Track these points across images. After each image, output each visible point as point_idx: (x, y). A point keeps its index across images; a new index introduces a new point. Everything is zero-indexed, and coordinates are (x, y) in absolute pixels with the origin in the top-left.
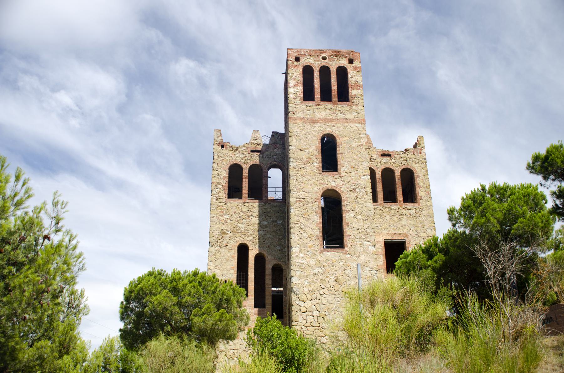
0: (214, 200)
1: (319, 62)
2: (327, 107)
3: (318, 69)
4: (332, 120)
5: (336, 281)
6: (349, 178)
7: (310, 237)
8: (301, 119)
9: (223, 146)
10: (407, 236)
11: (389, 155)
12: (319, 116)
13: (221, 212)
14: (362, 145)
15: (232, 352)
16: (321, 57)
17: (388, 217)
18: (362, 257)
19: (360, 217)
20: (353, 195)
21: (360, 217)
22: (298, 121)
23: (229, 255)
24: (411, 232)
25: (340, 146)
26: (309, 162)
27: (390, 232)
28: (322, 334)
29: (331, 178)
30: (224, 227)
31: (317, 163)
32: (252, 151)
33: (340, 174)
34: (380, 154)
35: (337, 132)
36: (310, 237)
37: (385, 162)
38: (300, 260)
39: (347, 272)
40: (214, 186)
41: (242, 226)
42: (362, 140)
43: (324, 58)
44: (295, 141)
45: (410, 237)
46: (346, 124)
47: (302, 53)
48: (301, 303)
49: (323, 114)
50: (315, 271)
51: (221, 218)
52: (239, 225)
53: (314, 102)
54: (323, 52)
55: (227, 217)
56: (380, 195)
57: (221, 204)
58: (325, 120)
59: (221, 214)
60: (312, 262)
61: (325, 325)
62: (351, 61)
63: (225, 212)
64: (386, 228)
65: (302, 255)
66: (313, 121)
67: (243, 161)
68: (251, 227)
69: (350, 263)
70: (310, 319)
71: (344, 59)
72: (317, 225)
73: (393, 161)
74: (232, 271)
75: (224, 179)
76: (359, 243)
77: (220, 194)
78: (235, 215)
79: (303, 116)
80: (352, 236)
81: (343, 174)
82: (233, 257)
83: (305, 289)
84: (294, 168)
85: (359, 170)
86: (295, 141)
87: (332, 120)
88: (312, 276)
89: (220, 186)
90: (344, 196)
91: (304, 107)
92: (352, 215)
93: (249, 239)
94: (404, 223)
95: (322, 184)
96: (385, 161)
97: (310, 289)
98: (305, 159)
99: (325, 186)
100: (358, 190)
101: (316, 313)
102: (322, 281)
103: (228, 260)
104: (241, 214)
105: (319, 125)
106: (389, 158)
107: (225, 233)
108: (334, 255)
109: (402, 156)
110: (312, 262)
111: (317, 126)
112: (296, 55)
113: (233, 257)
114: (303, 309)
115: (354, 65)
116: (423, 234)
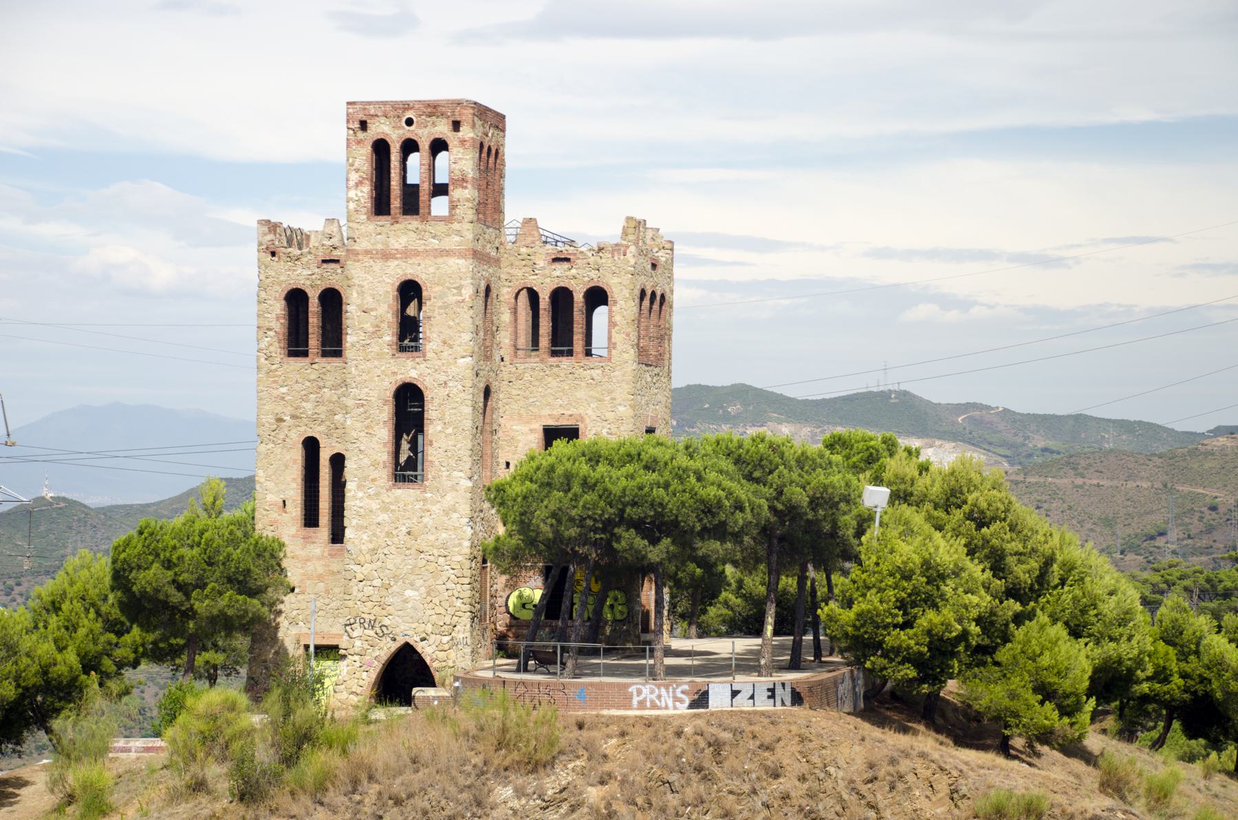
0: (262, 360)
1: (401, 132)
2: (410, 227)
3: (398, 146)
4: (417, 253)
5: (409, 533)
6: (439, 362)
7: (375, 464)
8: (367, 252)
9: (273, 254)
10: (582, 419)
11: (567, 260)
12: (397, 246)
13: (275, 382)
14: (463, 301)
15: (295, 613)
16: (404, 120)
17: (554, 383)
18: (449, 497)
19: (450, 430)
20: (443, 392)
21: (450, 430)
22: (360, 257)
23: (288, 457)
24: (590, 412)
25: (428, 303)
26: (377, 333)
27: (555, 413)
28: (384, 613)
29: (410, 363)
30: (279, 409)
31: (389, 336)
32: (324, 261)
33: (424, 356)
34: (550, 259)
35: (424, 276)
36: (375, 464)
37: (558, 276)
38: (358, 502)
39: (425, 520)
40: (261, 332)
41: (308, 406)
42: (463, 291)
43: (409, 122)
44: (355, 295)
45: (588, 421)
46: (440, 260)
47: (372, 112)
48: (356, 568)
49: (403, 240)
50: (380, 519)
51: (275, 393)
52: (304, 404)
53: (389, 218)
54: (407, 106)
55: (284, 390)
56: (545, 341)
57: (274, 367)
58: (407, 254)
59: (274, 385)
60: (374, 505)
61: (390, 600)
62: (456, 126)
63: (280, 382)
64: (549, 404)
65: (360, 494)
66: (386, 256)
67: (308, 283)
68: (324, 408)
69: (429, 506)
70: (369, 591)
71: (444, 121)
72: (385, 444)
73: (574, 271)
74: (294, 485)
75: (278, 318)
76: (446, 473)
77: (272, 349)
78: (296, 387)
79: (370, 247)
80: (437, 463)
81: (429, 355)
82: (295, 461)
83: (363, 547)
84: (353, 346)
85: (455, 347)
86: (355, 295)
87: (417, 253)
88: (374, 527)
89: (271, 333)
90: (428, 395)
91: (371, 227)
92: (439, 428)
93: (320, 429)
94: (580, 394)
95: (394, 373)
96: (558, 273)
97: (371, 546)
98: (371, 330)
99: (399, 377)
100: (450, 384)
101: (377, 582)
102: (389, 534)
103: (287, 466)
104: (308, 384)
105: (396, 262)
106: (566, 265)
107: (280, 420)
108: (406, 493)
109: (592, 260)
110: (374, 505)
111: (393, 264)
112: (362, 117)
113: (295, 461)
114: (360, 577)
115: (460, 134)
116: (610, 416)
